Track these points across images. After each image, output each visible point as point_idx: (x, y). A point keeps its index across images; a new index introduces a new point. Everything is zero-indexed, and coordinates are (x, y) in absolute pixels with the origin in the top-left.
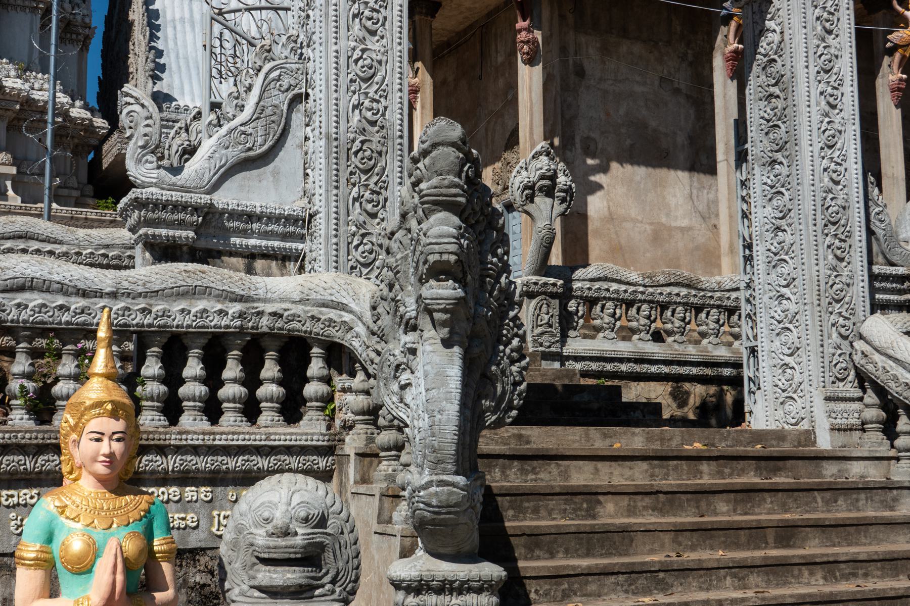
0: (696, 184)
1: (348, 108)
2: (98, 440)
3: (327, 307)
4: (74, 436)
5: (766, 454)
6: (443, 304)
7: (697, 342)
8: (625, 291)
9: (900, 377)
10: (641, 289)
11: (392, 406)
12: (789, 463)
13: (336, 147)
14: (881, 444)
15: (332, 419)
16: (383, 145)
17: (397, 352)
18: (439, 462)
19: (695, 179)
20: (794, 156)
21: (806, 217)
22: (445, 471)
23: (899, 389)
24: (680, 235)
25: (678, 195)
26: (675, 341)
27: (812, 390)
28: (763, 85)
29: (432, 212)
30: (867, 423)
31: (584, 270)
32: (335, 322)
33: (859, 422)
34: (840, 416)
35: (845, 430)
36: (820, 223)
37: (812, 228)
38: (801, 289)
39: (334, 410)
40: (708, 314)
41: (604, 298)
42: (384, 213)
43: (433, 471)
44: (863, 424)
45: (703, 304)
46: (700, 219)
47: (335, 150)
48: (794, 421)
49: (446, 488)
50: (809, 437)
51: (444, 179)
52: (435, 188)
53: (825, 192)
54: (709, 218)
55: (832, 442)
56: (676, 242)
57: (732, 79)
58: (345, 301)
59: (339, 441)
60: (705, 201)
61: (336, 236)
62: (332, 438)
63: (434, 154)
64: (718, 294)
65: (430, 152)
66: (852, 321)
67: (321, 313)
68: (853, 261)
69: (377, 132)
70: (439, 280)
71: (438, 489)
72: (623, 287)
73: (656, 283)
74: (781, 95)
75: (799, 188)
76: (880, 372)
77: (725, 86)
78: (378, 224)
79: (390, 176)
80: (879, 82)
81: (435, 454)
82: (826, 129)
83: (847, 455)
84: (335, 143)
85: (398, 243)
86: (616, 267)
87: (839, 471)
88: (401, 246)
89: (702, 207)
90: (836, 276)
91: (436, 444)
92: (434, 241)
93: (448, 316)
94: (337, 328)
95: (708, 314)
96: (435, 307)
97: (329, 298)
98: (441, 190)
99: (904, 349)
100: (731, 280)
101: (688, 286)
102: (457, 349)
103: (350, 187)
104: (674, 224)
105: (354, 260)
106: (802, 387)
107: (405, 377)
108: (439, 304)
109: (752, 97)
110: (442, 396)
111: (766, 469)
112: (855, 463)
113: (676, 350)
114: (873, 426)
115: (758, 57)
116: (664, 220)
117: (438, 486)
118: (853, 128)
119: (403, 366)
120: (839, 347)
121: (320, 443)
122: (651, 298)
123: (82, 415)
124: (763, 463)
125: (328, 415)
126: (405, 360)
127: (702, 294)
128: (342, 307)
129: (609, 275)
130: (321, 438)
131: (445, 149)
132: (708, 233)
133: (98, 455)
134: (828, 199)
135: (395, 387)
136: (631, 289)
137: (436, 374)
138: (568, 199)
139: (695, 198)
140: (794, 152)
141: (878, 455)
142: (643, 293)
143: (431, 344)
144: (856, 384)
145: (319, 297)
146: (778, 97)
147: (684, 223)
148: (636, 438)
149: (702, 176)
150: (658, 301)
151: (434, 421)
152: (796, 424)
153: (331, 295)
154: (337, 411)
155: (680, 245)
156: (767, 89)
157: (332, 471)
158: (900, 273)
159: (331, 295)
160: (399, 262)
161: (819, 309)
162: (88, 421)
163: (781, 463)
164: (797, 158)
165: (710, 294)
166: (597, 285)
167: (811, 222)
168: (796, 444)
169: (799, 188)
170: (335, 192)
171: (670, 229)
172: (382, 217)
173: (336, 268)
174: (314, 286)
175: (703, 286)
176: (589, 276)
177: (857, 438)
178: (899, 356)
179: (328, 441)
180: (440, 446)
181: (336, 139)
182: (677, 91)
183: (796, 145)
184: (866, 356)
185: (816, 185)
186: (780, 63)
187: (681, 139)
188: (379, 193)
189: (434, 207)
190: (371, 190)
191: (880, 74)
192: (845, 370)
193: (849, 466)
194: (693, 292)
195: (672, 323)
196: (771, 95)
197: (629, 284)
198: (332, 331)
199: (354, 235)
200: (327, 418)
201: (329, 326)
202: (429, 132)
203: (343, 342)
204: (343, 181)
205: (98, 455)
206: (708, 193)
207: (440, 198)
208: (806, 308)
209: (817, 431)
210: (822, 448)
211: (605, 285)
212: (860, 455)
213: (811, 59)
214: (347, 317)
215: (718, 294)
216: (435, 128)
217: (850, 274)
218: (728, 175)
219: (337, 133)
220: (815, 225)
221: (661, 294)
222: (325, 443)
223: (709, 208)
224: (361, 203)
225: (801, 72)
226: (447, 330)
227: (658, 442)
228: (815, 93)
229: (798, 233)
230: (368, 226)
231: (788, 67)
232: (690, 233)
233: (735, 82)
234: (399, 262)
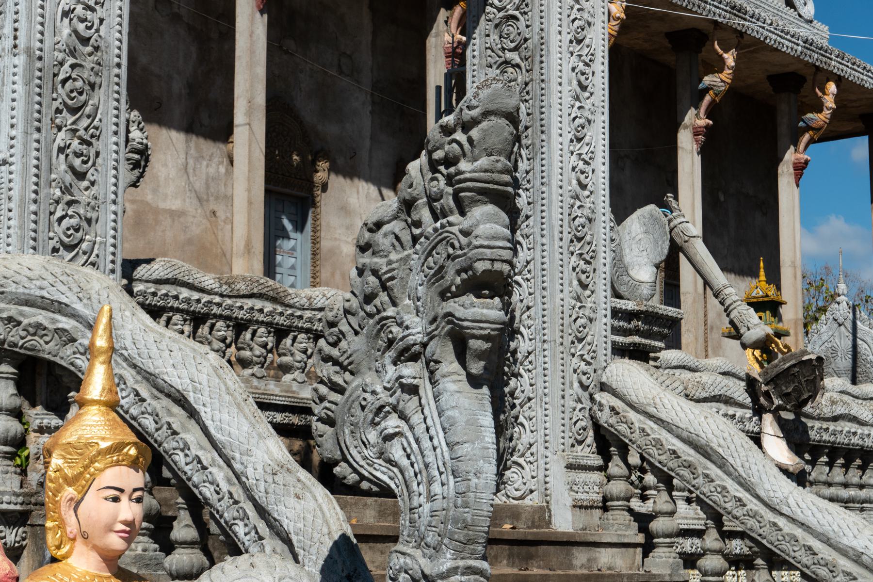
0: (193, 151)
1: (56, 14)
2: (116, 499)
3: (32, 306)
4: (70, 491)
5: (515, 537)
6: (487, 329)
7: (277, 379)
8: (198, 301)
9: (664, 443)
10: (217, 299)
11: (362, 463)
12: (543, 548)
13: (40, 70)
14: (628, 527)
15: (24, 473)
16: (97, 74)
17: (379, 388)
18: (470, 541)
19: (192, 145)
20: (538, 146)
21: (552, 228)
22: (473, 555)
23: (663, 458)
24: (169, 220)
25: (170, 165)
26: (253, 375)
27: (548, 454)
28: (495, 48)
29: (475, 202)
30: (612, 500)
31: (148, 267)
32: (45, 329)
33: (599, 498)
34: (581, 490)
35: (586, 508)
36: (567, 237)
37: (557, 243)
38: (539, 321)
39: (27, 458)
40: (294, 339)
41: (172, 309)
42: (95, 173)
43: (459, 553)
44: (605, 499)
45: (290, 326)
46: (195, 201)
47: (38, 74)
48: (518, 494)
49: (472, 577)
50: (543, 515)
51: (497, 161)
52: (486, 171)
53: (572, 197)
54: (208, 200)
55: (573, 523)
56: (163, 231)
57: (262, 12)
58: (64, 300)
59: (36, 504)
60: (204, 177)
61: (35, 201)
62: (27, 499)
63: (484, 124)
64: (308, 314)
65: (479, 122)
66: (593, 367)
67: (21, 314)
68: (597, 290)
69: (90, 55)
70: (478, 296)
71: (463, 578)
72: (196, 296)
73: (235, 293)
74: (522, 65)
75: (544, 189)
76: (636, 435)
77: (252, 21)
78: (87, 189)
79: (104, 121)
80: (431, 41)
81: (465, 531)
82: (576, 117)
83: (591, 539)
84: (39, 64)
85: (391, 239)
86: (187, 266)
87: (589, 560)
88: (397, 244)
89: (199, 185)
90: (580, 308)
91: (468, 517)
92: (486, 243)
93: (489, 345)
94: (47, 339)
95: (294, 339)
96: (475, 332)
97: (38, 293)
98: (493, 175)
99: (669, 407)
100: (324, 296)
101: (274, 300)
102: (485, 390)
103: (55, 130)
104: (162, 205)
105: (56, 239)
106: (533, 449)
107: (392, 423)
108: (481, 328)
109: (476, 61)
110: (477, 452)
111: (518, 557)
112: (603, 550)
113: (257, 388)
114: (620, 503)
115: (488, 9)
116: (149, 198)
117: (463, 574)
118: (603, 118)
119: (387, 409)
120: (579, 401)
121: (12, 507)
122: (227, 313)
123: (92, 461)
124: (516, 548)
125: (18, 466)
126: (392, 400)
127: (290, 311)
128: (61, 308)
129: (179, 277)
130: (13, 499)
131: (499, 121)
132: (204, 221)
133: (115, 521)
134: (576, 207)
135: (372, 436)
136: (206, 298)
137: (467, 422)
138: (143, 163)
139: (191, 171)
140: (538, 142)
141: (626, 541)
142: (219, 305)
143: (454, 382)
144: (594, 449)
145: (21, 290)
146: (518, 66)
147: (175, 204)
148: (367, 511)
149: (202, 141)
150: (236, 318)
151: (469, 487)
152: (522, 498)
153: (41, 288)
154: (31, 460)
155: (169, 234)
156: (501, 53)
157: (22, 548)
158: (629, 308)
159: (41, 288)
160: (394, 266)
161: (561, 349)
162: (101, 470)
163: (532, 549)
164: (544, 150)
165: (299, 313)
166: (164, 290)
167: (557, 236)
168: (530, 524)
169: (544, 189)
170: (36, 136)
171: (156, 211)
172: (92, 179)
173: (34, 248)
174: (12, 273)
175: (292, 302)
176: (154, 276)
177: (598, 519)
178: (663, 416)
179: (22, 504)
180: (473, 520)
181: (40, 58)
182: (176, 18)
183: (542, 132)
184: (618, 413)
185: (564, 187)
186: (522, 23)
187: (178, 86)
188: (89, 144)
189: (479, 197)
190: (80, 138)
191: (434, 31)
192: (584, 430)
193: (597, 554)
194: (280, 309)
195: (251, 349)
196: (507, 62)
197: (202, 290)
198: (37, 342)
199: (57, 202)
200: (18, 470)
201: (34, 334)
202: (481, 96)
203: (57, 360)
204: (46, 121)
205: (115, 521)
206: (207, 166)
207: (490, 186)
208: (546, 346)
209: (552, 508)
210: (560, 530)
211: (173, 290)
212: (609, 540)
213: (565, 23)
214: (65, 323)
215: (308, 314)
216: (490, 90)
217: (594, 306)
218: (250, 145)
219: (41, 50)
220: (561, 239)
221: (241, 308)
222: (18, 507)
223: (208, 187)
224: (67, 156)
225: (553, 39)
226: (482, 363)
227: (391, 518)
228: (567, 68)
229: (539, 248)
230: (75, 191)
231: (536, 27)
232: (182, 219)
233: (266, 16)
234: (394, 266)
